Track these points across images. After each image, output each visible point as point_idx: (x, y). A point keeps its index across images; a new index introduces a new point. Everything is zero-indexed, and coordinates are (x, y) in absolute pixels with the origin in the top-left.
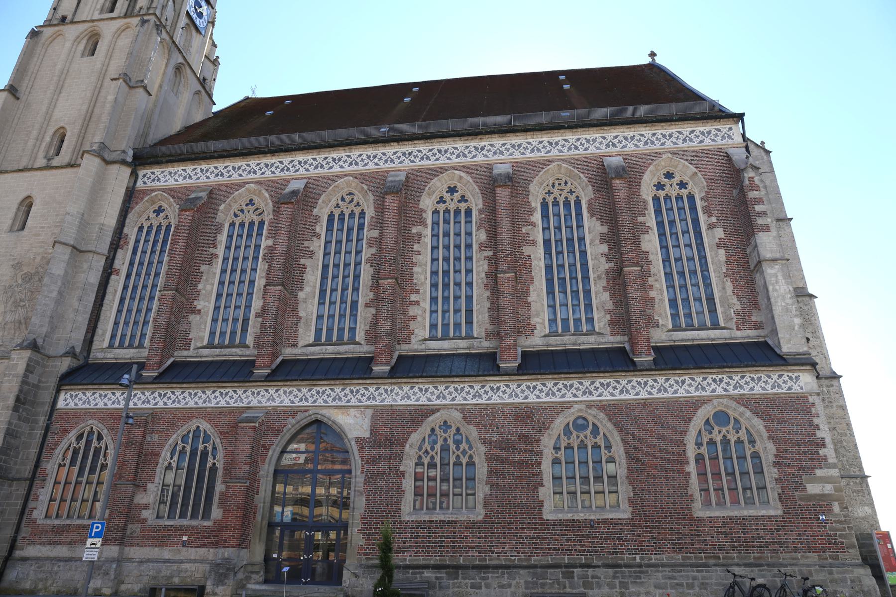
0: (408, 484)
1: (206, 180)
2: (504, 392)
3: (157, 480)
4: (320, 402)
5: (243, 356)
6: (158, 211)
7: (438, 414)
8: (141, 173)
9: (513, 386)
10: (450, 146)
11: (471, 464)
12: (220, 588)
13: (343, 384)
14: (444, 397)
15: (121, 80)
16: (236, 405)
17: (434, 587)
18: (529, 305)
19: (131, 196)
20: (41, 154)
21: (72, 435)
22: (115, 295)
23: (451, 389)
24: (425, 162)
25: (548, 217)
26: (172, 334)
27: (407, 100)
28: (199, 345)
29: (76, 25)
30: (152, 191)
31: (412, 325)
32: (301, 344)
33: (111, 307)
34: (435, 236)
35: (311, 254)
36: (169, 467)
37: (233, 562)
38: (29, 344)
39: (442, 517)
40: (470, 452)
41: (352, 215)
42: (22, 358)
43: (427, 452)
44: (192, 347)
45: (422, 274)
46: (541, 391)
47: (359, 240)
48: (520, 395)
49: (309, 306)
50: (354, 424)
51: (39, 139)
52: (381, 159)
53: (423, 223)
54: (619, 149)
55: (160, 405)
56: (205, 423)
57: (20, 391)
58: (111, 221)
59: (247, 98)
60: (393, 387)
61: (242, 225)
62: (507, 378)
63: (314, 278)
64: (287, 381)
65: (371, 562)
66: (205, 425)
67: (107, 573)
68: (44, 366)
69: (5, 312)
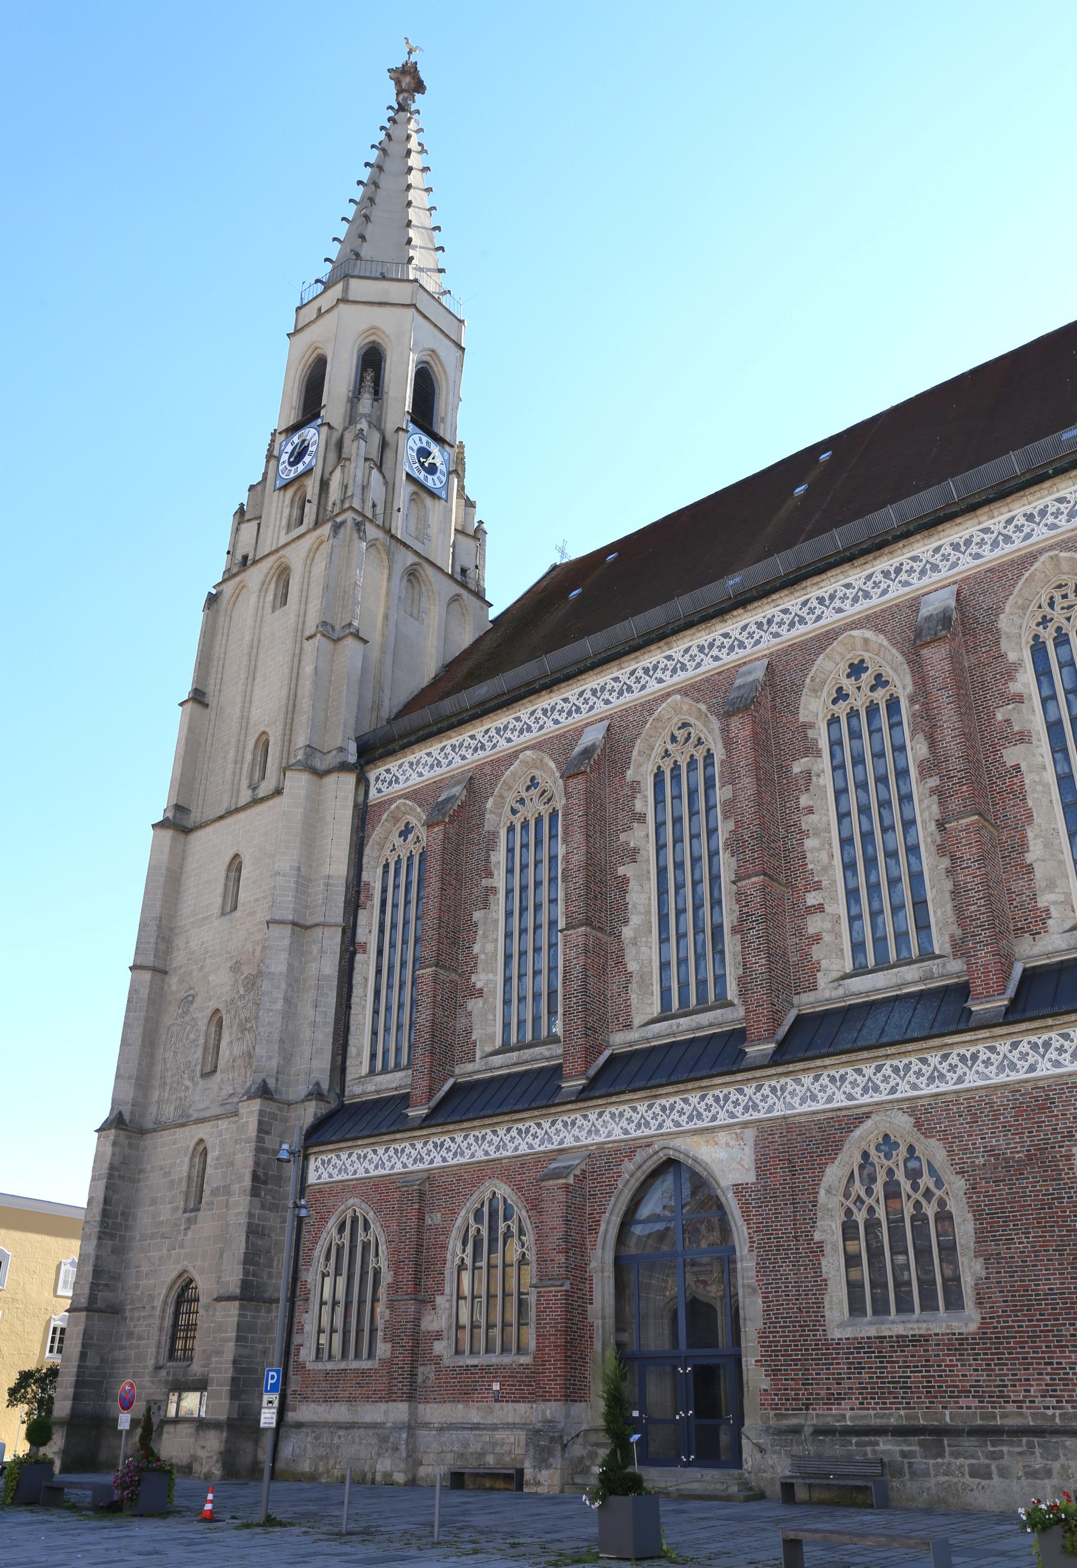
0: (833, 1267)
1: (462, 763)
2: (987, 1063)
3: (447, 1290)
4: (669, 1126)
5: (551, 1058)
6: (404, 833)
7: (869, 1122)
8: (372, 776)
9: (1003, 1047)
10: (837, 586)
11: (944, 1217)
12: (544, 1472)
13: (702, 1088)
14: (876, 1089)
15: (319, 636)
16: (542, 1148)
17: (901, 1473)
18: (1029, 869)
19: (364, 816)
20: (245, 783)
21: (332, 1225)
22: (366, 987)
23: (887, 1070)
24: (800, 630)
25: (1049, 673)
26: (444, 1040)
27: (799, 490)
28: (489, 1049)
29: (259, 565)
30: (391, 801)
31: (817, 952)
32: (637, 1021)
33: (364, 1007)
34: (838, 768)
35: (1024, 738)
36: (461, 1267)
37: (560, 1426)
38: (258, 1089)
39: (900, 1330)
40: (938, 1193)
41: (692, 764)
42: (251, 1112)
43: (859, 1200)
44: (478, 1055)
45: (822, 850)
46: (919, 1074)
47: (709, 808)
48: (1020, 1064)
49: (644, 949)
50: (728, 1161)
51: (238, 761)
52: (844, 598)
53: (811, 750)
54: (945, 573)
55: (438, 1163)
56: (503, 1185)
57: (257, 1164)
58: (338, 866)
59: (554, 568)
60: (783, 1081)
61: (525, 826)
62: (985, 1033)
63: (644, 896)
64: (611, 1095)
65: (785, 1422)
66: (503, 1190)
67: (396, 1449)
68: (285, 1120)
69: (231, 1042)
